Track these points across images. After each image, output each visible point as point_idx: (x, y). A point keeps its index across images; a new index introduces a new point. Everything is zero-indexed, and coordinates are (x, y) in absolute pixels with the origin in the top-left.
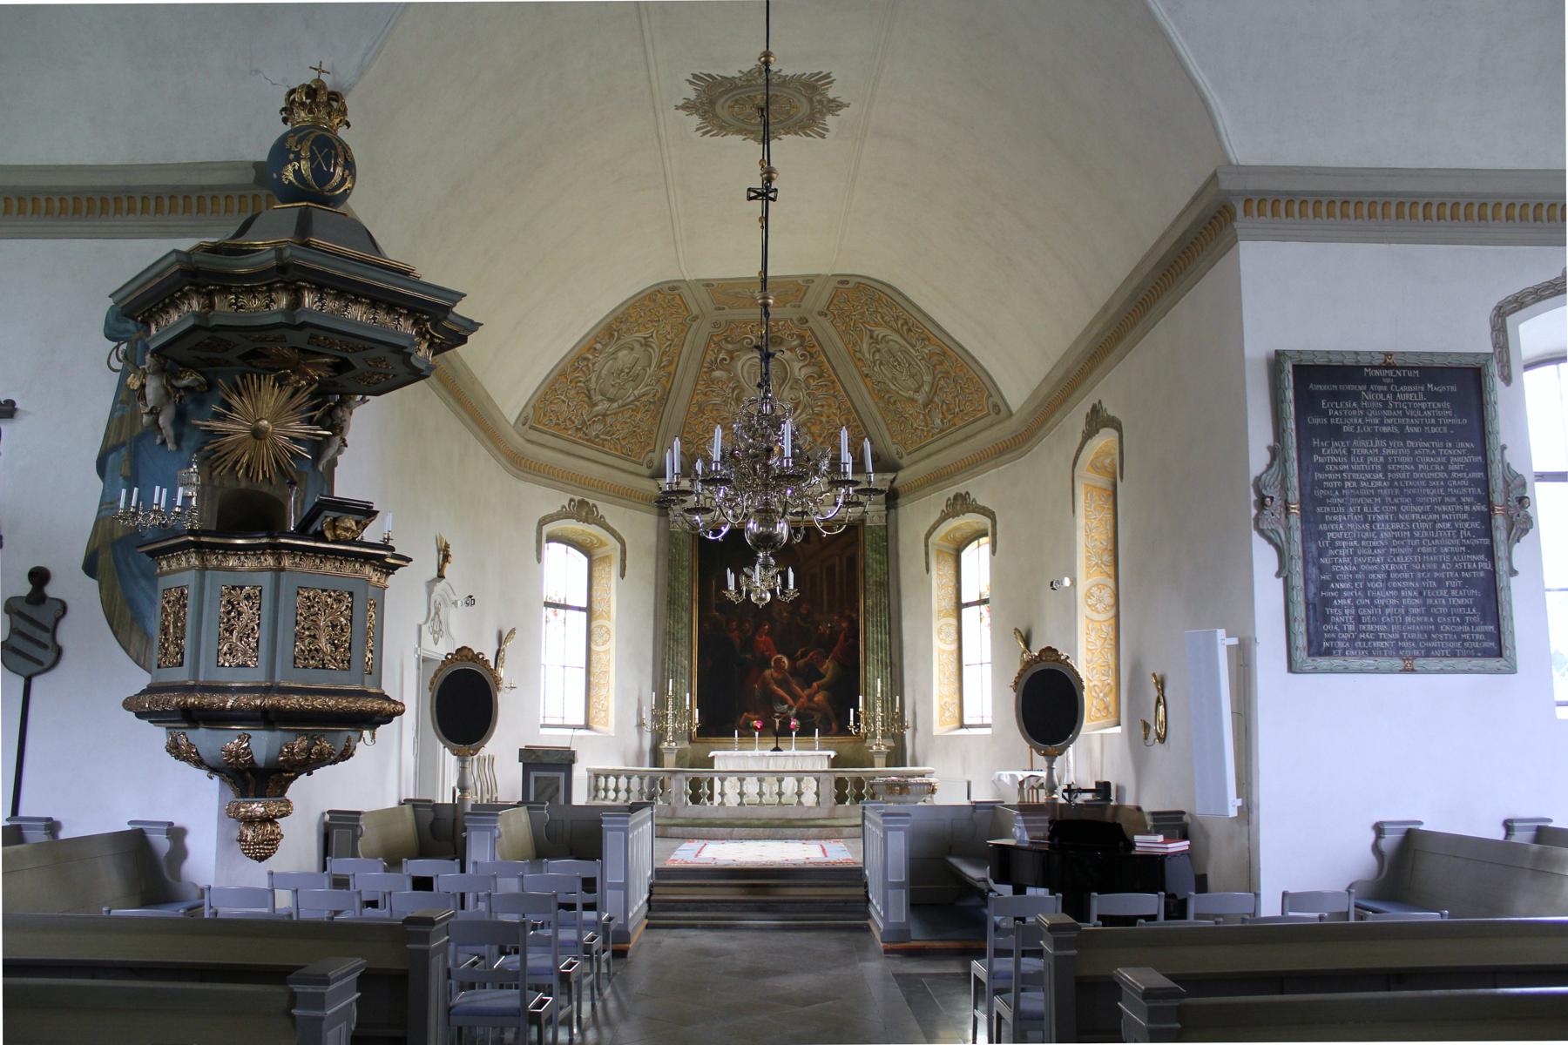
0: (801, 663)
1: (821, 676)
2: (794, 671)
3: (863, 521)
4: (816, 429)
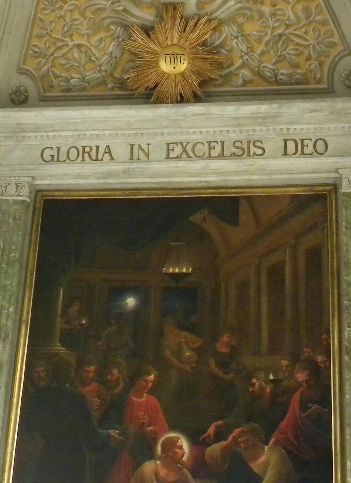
3: (335, 186)
4: (252, 29)
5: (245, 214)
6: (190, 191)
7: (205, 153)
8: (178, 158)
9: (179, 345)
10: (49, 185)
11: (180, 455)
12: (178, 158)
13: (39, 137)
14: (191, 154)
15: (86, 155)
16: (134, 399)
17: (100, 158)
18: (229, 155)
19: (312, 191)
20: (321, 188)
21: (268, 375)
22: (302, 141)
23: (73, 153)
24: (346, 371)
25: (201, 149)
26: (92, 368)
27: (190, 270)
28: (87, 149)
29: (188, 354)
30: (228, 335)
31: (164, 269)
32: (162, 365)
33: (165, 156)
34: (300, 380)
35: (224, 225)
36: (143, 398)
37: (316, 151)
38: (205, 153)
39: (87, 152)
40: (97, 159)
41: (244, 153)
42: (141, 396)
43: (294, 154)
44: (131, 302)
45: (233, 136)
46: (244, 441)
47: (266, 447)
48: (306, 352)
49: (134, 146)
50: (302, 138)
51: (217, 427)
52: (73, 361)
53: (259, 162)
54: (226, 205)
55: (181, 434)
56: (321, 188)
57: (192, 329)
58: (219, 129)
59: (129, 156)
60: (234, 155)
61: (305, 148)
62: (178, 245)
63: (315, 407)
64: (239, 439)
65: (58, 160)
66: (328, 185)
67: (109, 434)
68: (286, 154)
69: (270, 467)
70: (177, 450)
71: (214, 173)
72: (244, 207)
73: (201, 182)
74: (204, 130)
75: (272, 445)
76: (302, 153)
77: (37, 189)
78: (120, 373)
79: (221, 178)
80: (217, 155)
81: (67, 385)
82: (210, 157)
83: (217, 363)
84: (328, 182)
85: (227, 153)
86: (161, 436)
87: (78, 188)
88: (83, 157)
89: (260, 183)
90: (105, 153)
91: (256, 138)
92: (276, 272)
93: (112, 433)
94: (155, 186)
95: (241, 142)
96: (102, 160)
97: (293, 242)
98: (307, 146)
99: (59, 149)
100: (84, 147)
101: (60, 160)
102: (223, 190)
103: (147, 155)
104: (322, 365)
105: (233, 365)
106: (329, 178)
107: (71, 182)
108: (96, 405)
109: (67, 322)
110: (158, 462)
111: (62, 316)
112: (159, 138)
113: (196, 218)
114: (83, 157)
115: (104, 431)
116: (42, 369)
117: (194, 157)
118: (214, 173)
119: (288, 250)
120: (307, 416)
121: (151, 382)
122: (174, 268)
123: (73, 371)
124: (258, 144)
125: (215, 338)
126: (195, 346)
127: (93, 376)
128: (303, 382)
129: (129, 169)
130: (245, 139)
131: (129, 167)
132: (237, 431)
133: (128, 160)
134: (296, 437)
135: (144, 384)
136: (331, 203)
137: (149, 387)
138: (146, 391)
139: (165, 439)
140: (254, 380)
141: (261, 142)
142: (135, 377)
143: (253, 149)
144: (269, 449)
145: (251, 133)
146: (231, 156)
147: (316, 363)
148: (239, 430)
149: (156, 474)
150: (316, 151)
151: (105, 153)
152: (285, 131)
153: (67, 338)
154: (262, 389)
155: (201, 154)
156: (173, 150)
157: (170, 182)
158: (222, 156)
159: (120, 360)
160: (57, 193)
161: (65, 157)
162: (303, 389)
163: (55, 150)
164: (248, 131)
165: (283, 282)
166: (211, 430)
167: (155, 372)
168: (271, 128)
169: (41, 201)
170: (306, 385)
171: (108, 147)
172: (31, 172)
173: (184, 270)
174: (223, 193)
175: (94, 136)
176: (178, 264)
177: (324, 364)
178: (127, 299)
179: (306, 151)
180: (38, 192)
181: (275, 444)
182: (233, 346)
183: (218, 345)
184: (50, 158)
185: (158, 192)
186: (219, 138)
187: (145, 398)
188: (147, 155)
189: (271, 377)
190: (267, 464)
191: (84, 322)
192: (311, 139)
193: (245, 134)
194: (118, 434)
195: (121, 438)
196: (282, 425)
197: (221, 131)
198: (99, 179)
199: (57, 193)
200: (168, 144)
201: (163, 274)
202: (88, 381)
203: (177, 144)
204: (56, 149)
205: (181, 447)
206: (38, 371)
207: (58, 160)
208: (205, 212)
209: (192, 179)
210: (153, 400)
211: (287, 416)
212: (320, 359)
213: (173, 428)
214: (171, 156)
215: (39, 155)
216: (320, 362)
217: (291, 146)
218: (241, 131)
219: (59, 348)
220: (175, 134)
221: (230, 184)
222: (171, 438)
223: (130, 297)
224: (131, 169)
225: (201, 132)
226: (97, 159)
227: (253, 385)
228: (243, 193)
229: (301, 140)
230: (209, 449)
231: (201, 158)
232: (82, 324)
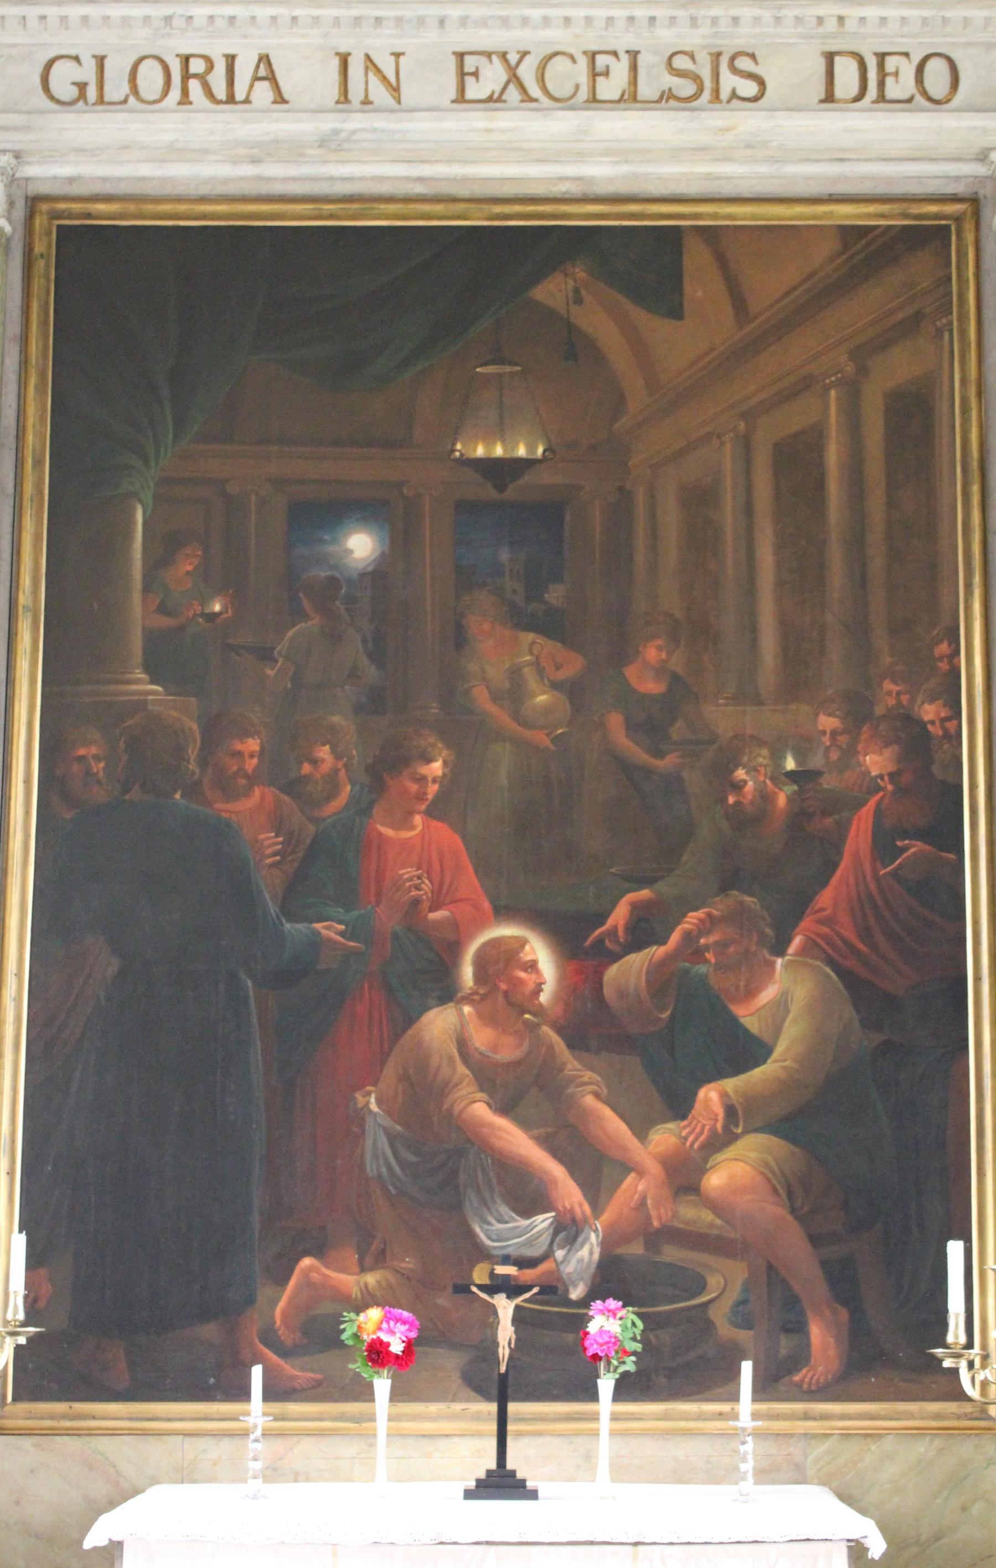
0: (629, 971)
1: (744, 1051)
2: (590, 1023)
5: (701, 283)
6: (531, 208)
7: (577, 87)
8: (494, 100)
9: (515, 673)
10: (71, 180)
11: (531, 986)
12: (494, 100)
13: (33, 22)
14: (535, 91)
15: (194, 85)
16: (383, 829)
17: (240, 96)
18: (656, 96)
19: (905, 216)
20: (933, 209)
21: (778, 757)
22: (881, 57)
23: (151, 77)
25: (566, 76)
26: (253, 744)
27: (540, 450)
28: (197, 66)
29: (542, 698)
30: (659, 642)
31: (459, 446)
32: (464, 731)
33: (453, 94)
34: (873, 774)
35: (639, 316)
36: (413, 827)
37: (924, 93)
38: (577, 87)
39: (195, 76)
40: (231, 99)
41: (701, 90)
42: (405, 823)
43: (858, 99)
44: (361, 546)
45: (668, 37)
46: (716, 943)
47: (779, 962)
48: (890, 692)
49: (350, 59)
50: (460, 49)
51: (635, 906)
53: (749, 122)
54: (644, 254)
55: (532, 929)
56: (933, 209)
57: (551, 625)
58: (626, 13)
59: (335, 93)
60: (667, 96)
61: (889, 81)
62: (500, 375)
63: (916, 847)
64: (702, 941)
65: (101, 100)
66: (955, 199)
68: (829, 97)
69: (791, 1016)
70: (522, 974)
71: (607, 152)
72: (696, 258)
73: (561, 179)
74: (578, 13)
75: (796, 954)
76: (882, 97)
77: (30, 193)
78: (338, 757)
79: (624, 169)
80: (616, 96)
81: (178, 796)
82: (593, 100)
83: (632, 727)
84: (950, 189)
85: (646, 90)
86: (471, 936)
87: (168, 190)
88: (185, 92)
89: (745, 189)
90: (256, 78)
91: (739, 43)
92: (798, 462)
93: (324, 932)
94: (419, 189)
95: (692, 57)
96: (247, 101)
97: (850, 368)
98: (896, 74)
99: (101, 61)
100: (186, 60)
101: (106, 99)
102: (548, 208)
103: (395, 90)
104: (935, 730)
105: (678, 730)
106: (957, 179)
107: (146, 170)
108: (268, 851)
109: (162, 609)
110: (467, 1009)
111: (146, 589)
112: (431, 35)
113: (552, 291)
114: (185, 92)
115: (301, 926)
116: (94, 750)
117: (545, 101)
118: (607, 152)
119: (833, 393)
120: (895, 874)
121: (434, 781)
122: (489, 445)
123: (192, 753)
124: (744, 64)
125: (621, 651)
126: (561, 675)
127: (257, 767)
128: (881, 777)
129: (336, 132)
130: (704, 47)
131: (337, 125)
132: (692, 919)
133: (331, 104)
134: (865, 933)
135: (414, 787)
136: (962, 254)
137: (430, 797)
138: (423, 807)
139: (484, 945)
140: (740, 774)
141: (753, 56)
143: (729, 81)
144: (786, 966)
145: (724, 27)
146: (659, 101)
147: (922, 725)
148: (700, 914)
149: (462, 1044)
150: (924, 93)
151: (256, 78)
152: (831, 25)
154: (765, 798)
155: (566, 91)
156: (476, 74)
157: (466, 179)
158: (630, 98)
160: (102, 207)
161: (125, 88)
162: (882, 798)
163: (90, 66)
164: (715, 21)
165: (821, 486)
166: (620, 915)
167: (445, 753)
168: (789, 14)
169: (49, 233)
170: (890, 787)
171: (264, 59)
172: (14, 136)
173: (522, 452)
174: (632, 216)
175: (219, 23)
176: (500, 431)
177: (943, 728)
178: (349, 534)
179: (893, 90)
180: (34, 202)
181: (802, 952)
182: (675, 678)
183: (631, 672)
184: (75, 91)
185: (427, 208)
186: (623, 42)
187: (420, 828)
188: (395, 90)
189: (790, 764)
190: (782, 1005)
191: (217, 608)
192: (907, 55)
193: (706, 30)
194: (342, 934)
195: (352, 944)
196: (825, 899)
197: (631, 19)
198: (235, 163)
199: (102, 207)
200: (460, 56)
201: (456, 460)
203: (489, 55)
204: (93, 62)
205: (532, 966)
206: (81, 759)
207: (101, 100)
208: (580, 273)
209: (533, 171)
210: (444, 834)
211: (838, 873)
212: (929, 712)
213: (504, 912)
214: (470, 95)
215: (37, 79)
216: (932, 722)
217: (846, 73)
218: (778, 19)
219: (143, 686)
220: (484, 23)
221: (654, 189)
222: (495, 943)
223: (358, 532)
224: (343, 135)
225: (567, 20)
226: (231, 99)
227: (738, 787)
228: (697, 216)
229: (876, 54)
230: (612, 972)
231: (563, 102)
232: (213, 617)
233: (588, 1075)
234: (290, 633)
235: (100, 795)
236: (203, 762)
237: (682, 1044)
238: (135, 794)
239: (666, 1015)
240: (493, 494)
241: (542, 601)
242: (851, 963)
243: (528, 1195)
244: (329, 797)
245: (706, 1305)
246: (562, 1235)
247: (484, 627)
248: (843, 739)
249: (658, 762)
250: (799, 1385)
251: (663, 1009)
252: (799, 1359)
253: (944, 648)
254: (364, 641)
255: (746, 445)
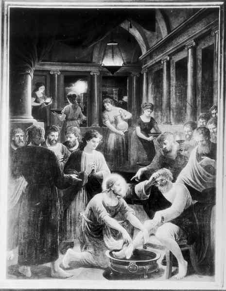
0: (140, 187)
1: (166, 204)
2: (131, 199)
21: (174, 137)
24: (81, 194)
32: (106, 132)
48: (200, 122)
52: (43, 129)
57: (124, 106)
63: (206, 158)
67: (71, 177)
72: (159, 17)
97: (194, 44)
105: (153, 131)
108: (61, 158)
113: (125, 26)
116: (21, 134)
125: (139, 112)
138: (95, 148)
142: (87, 137)
153: (38, 113)
159: (76, 128)
166: (139, 174)
182: (152, 118)
194: (77, 177)
202: (54, 142)
233: (132, 209)
234: (65, 108)
235: (22, 144)
236: (46, 138)
237: (153, 202)
238: (30, 144)
239: (148, 196)
240: (111, 75)
241: (122, 100)
242: (190, 185)
243: (116, 234)
244: (74, 146)
245: (156, 261)
246: (125, 245)
247: (109, 106)
248: (190, 133)
249: (148, 138)
250: (176, 278)
251: (147, 195)
252: (176, 272)
253: (214, 111)
254: (82, 109)
255: (169, 63)
